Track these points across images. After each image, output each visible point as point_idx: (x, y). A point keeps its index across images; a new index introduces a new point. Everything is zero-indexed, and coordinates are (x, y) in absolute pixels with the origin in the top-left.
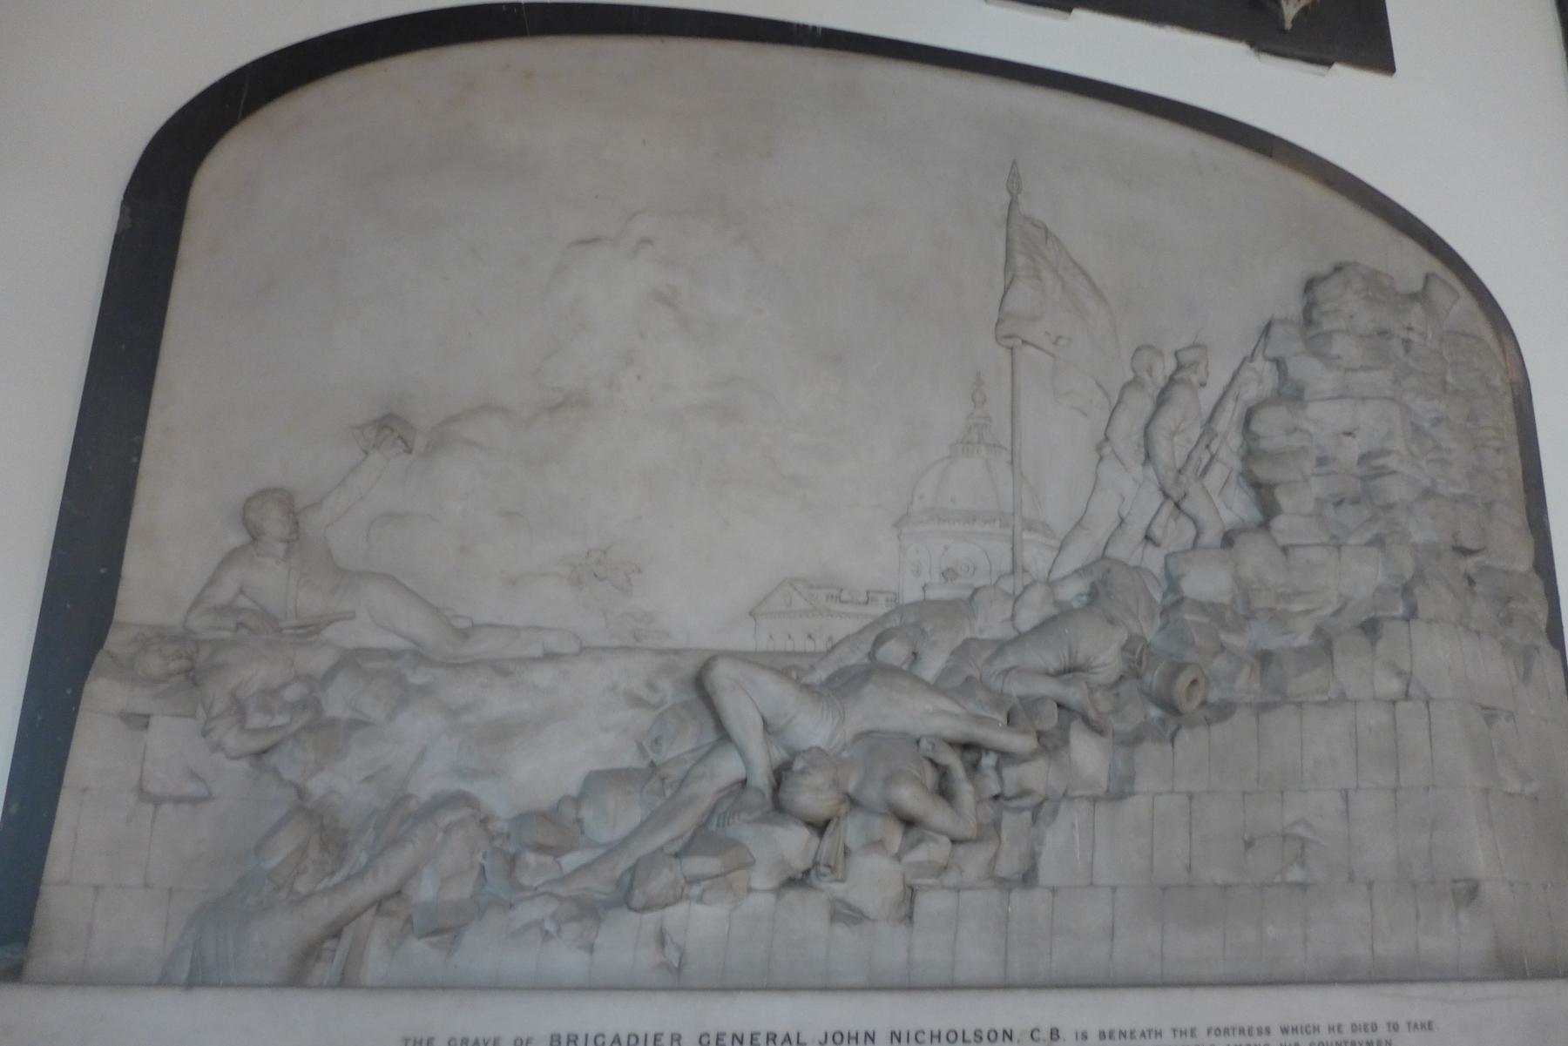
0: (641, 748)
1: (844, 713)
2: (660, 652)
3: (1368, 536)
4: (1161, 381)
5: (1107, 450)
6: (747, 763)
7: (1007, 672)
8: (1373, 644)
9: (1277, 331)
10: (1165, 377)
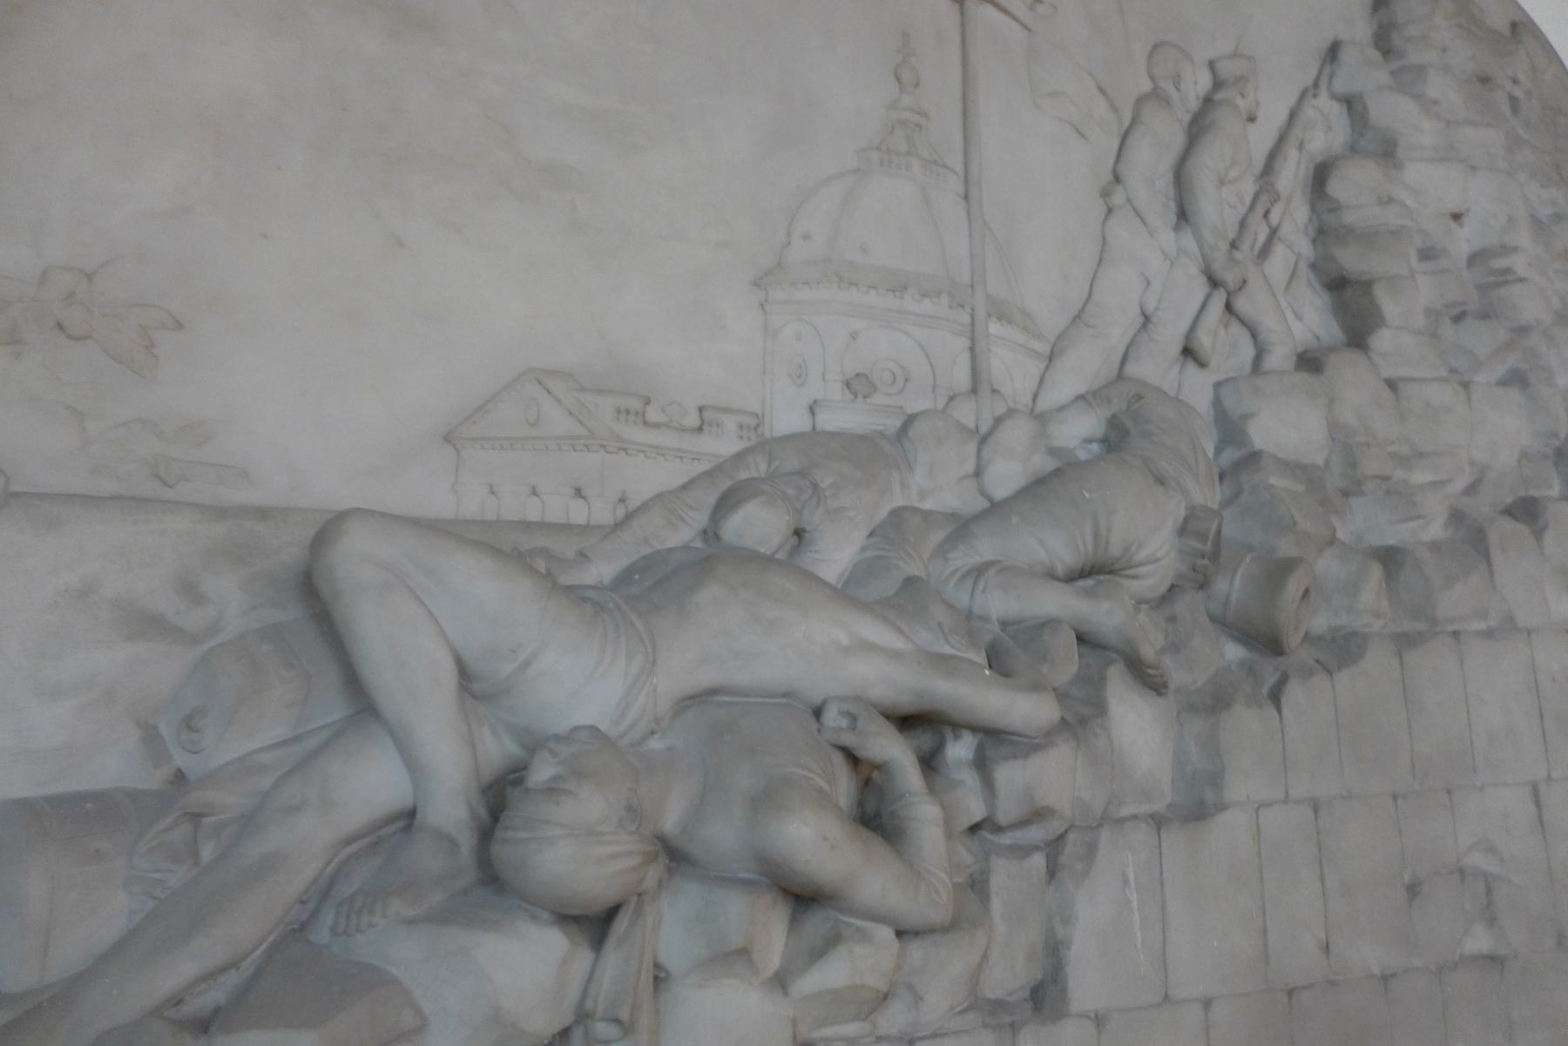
0: (151, 737)
1: (654, 647)
2: (221, 513)
3: (1500, 371)
4: (1194, 105)
5: (1118, 198)
6: (414, 767)
7: (979, 571)
8: (1538, 534)
9: (1348, 56)
10: (1198, 97)
